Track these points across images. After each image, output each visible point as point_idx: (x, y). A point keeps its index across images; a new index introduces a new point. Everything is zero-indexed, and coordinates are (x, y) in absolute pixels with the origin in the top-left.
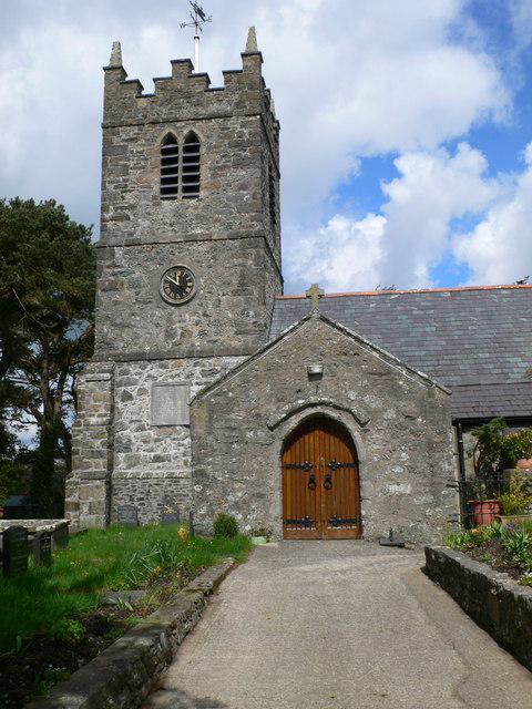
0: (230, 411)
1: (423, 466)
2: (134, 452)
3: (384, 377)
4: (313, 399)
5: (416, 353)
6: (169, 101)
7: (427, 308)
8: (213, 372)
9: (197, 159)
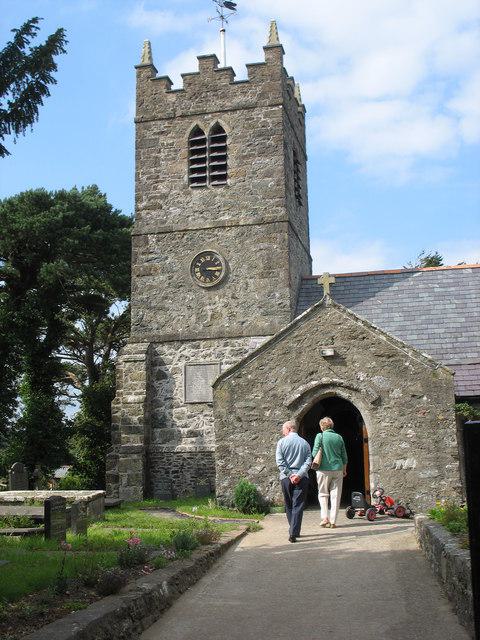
0: (250, 391)
1: (427, 441)
2: (169, 428)
3: (391, 359)
4: (325, 380)
5: (436, 331)
6: (195, 95)
7: (449, 285)
8: (240, 352)
9: (224, 149)
